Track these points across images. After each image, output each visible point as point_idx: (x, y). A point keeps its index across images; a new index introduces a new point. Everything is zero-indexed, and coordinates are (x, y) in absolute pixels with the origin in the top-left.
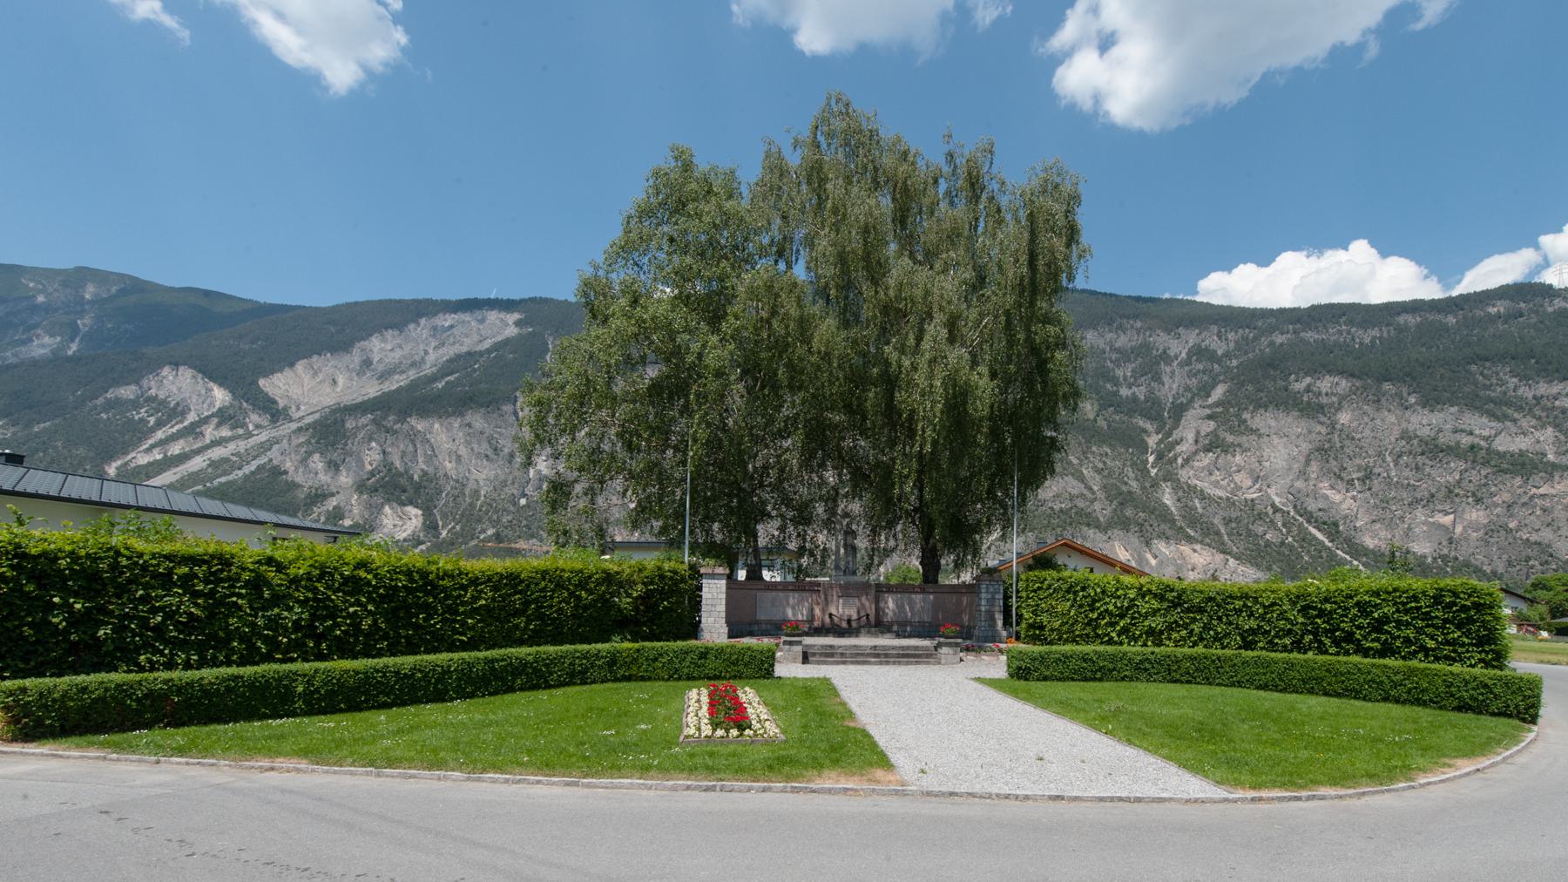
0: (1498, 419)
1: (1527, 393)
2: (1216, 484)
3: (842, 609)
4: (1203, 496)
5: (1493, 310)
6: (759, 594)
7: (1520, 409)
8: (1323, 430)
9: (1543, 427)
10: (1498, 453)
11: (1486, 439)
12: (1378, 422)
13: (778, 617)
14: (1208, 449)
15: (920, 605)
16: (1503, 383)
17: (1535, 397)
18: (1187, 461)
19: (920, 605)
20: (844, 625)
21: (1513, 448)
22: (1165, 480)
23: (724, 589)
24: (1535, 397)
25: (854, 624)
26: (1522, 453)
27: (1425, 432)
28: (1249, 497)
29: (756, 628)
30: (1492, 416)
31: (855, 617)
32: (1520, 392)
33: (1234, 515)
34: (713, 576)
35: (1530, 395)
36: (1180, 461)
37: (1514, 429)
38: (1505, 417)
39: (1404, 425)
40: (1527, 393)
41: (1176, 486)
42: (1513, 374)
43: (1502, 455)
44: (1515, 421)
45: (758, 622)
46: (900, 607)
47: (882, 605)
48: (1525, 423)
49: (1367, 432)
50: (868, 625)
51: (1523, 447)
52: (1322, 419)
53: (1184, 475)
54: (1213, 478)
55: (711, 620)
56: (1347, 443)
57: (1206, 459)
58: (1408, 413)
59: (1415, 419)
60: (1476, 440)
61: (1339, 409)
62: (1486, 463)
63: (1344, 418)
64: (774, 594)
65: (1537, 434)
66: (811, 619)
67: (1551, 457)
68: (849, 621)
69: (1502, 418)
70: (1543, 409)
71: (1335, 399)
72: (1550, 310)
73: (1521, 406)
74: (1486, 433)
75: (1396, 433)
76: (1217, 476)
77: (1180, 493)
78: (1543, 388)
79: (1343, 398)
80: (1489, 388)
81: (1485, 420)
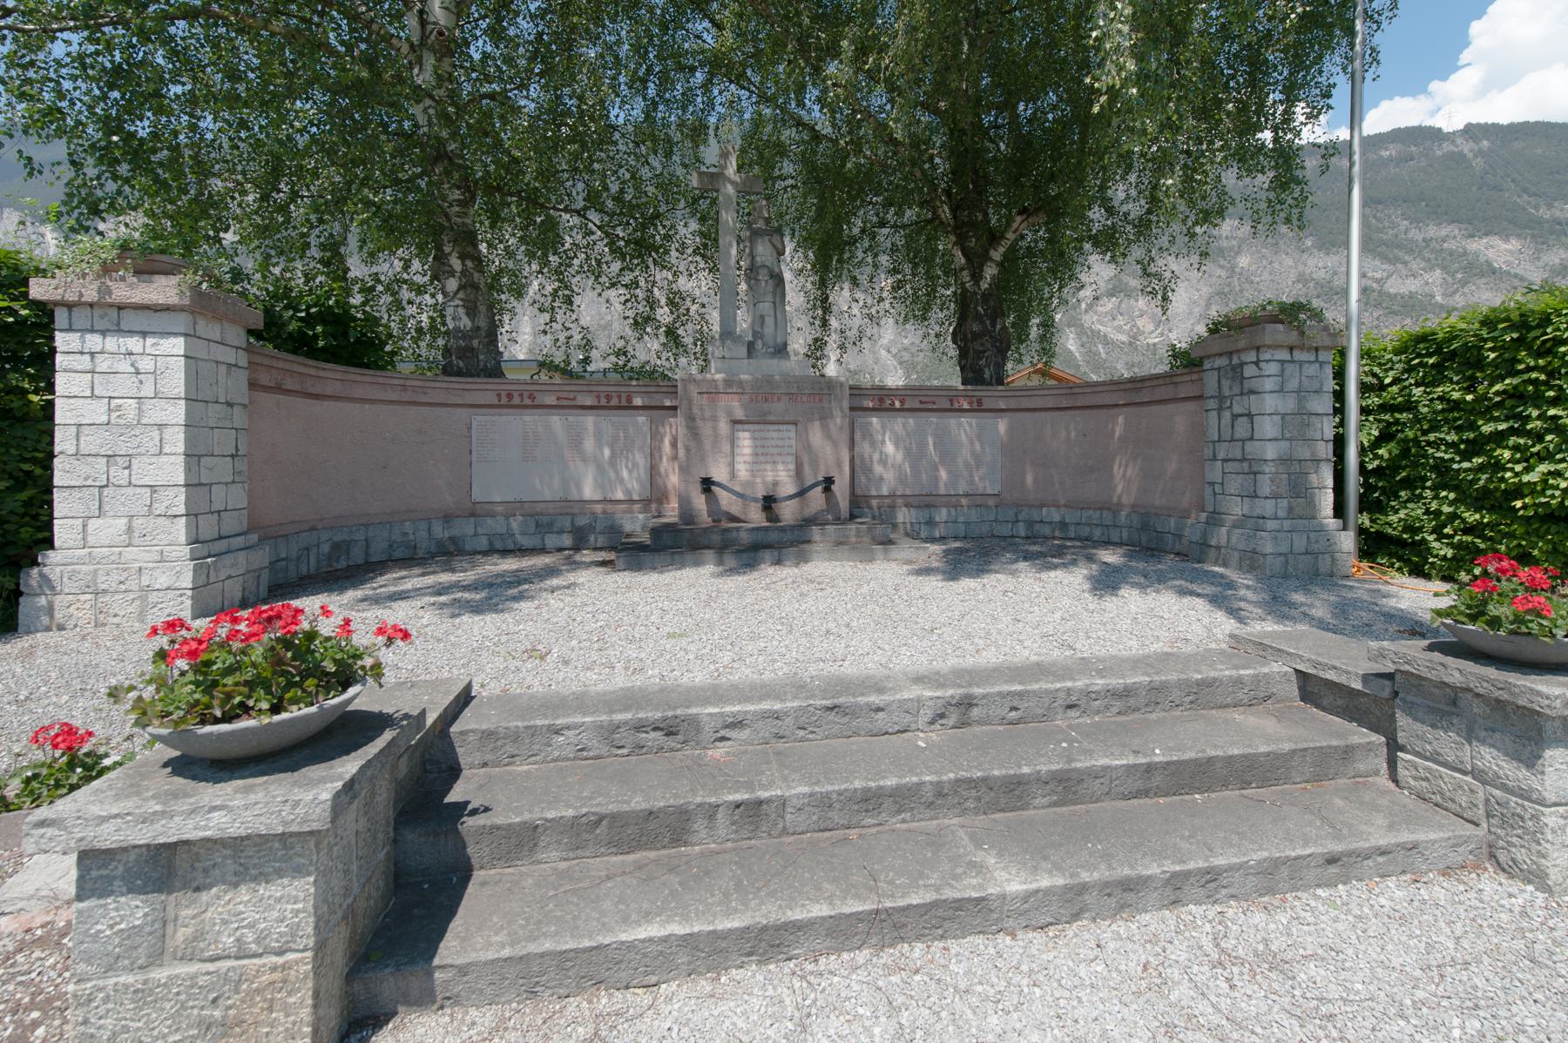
0: (1390, 261)
1: (1416, 235)
2: (1119, 329)
3: (747, 465)
4: (1106, 341)
5: (1385, 154)
6: (479, 420)
7: (1410, 251)
8: (1223, 274)
9: (1432, 269)
10: (1389, 295)
11: (1378, 281)
12: (1276, 265)
13: (546, 489)
14: (1111, 294)
15: (971, 451)
16: (1394, 226)
17: (1424, 240)
18: (1090, 306)
19: (971, 451)
20: (756, 516)
21: (1404, 290)
22: (1069, 326)
23: (176, 380)
24: (1424, 240)
25: (788, 512)
26: (1412, 295)
27: (1322, 274)
28: (1151, 341)
29: (464, 528)
30: (1385, 258)
31: (788, 488)
32: (1410, 235)
33: (1136, 360)
34: (115, 317)
35: (1420, 238)
36: (1083, 306)
37: (1404, 272)
38: (1396, 260)
39: (1301, 268)
40: (1416, 235)
41: (1081, 331)
42: (1405, 217)
43: (1393, 297)
44: (1405, 263)
45: (475, 512)
46: (915, 456)
47: (864, 448)
48: (1415, 266)
49: (1266, 276)
50: (831, 517)
51: (1413, 288)
52: (1222, 262)
53: (1088, 320)
54: (1116, 323)
55: (107, 530)
56: (1247, 286)
57: (1108, 305)
58: (1305, 256)
59: (1311, 262)
60: (1369, 283)
61: (1238, 253)
62: (1377, 305)
63: (1243, 261)
64: (530, 419)
65: (1426, 276)
66: (655, 496)
67: (1438, 298)
68: (769, 502)
69: (1393, 261)
70: (1432, 251)
71: (1234, 243)
72: (1439, 153)
73: (1412, 248)
74: (1378, 275)
75: (1293, 277)
76: (1120, 320)
77: (1084, 339)
78: (1432, 231)
79: (1242, 241)
80: (1381, 230)
81: (1377, 262)
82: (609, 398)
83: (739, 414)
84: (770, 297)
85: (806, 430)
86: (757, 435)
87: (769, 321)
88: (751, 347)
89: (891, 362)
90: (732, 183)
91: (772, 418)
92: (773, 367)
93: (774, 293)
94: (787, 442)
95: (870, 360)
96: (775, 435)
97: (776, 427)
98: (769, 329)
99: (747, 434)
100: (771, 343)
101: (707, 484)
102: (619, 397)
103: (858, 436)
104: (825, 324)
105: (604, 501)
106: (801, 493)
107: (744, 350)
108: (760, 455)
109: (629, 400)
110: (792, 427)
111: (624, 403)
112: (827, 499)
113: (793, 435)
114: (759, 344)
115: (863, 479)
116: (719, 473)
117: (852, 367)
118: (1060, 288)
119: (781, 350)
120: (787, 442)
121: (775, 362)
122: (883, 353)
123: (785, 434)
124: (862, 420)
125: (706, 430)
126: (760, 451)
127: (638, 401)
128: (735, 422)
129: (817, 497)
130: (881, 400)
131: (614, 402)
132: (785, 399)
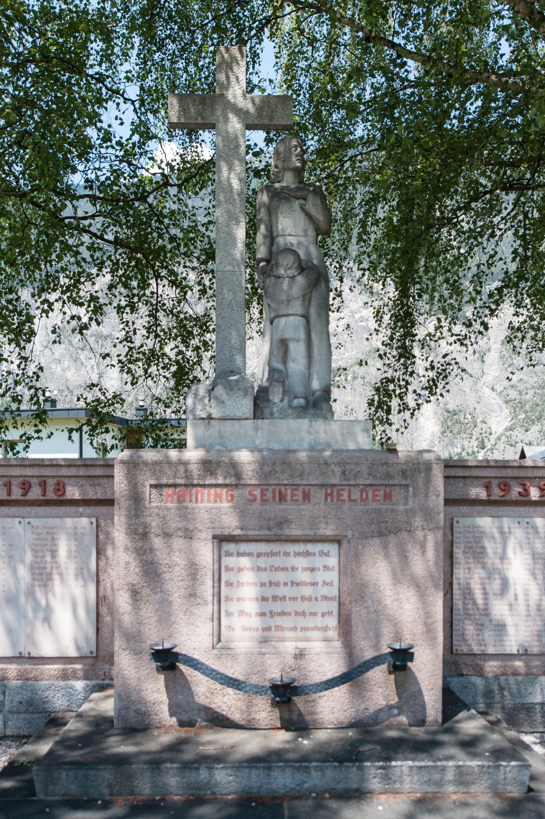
31: (326, 662)
47: (471, 576)
82: (26, 487)
83: (230, 523)
84: (297, 307)
85: (357, 556)
86: (262, 562)
87: (297, 350)
88: (261, 402)
89: (495, 400)
90: (239, 112)
91: (296, 532)
92: (299, 434)
93: (306, 298)
94: (320, 576)
95: (471, 399)
96: (301, 562)
97: (300, 547)
98: (297, 365)
99: (245, 562)
100: (299, 388)
101: (167, 660)
102: (43, 485)
103: (458, 553)
104: (406, 354)
105: (19, 658)
106: (353, 675)
107: (245, 406)
108: (271, 604)
109: (60, 488)
110: (333, 548)
111: (51, 495)
112: (400, 687)
113: (333, 561)
114: (276, 397)
115: (470, 629)
116: (192, 638)
117: (451, 407)
118: (185, 399)
119: (318, 403)
120: (320, 576)
121: (304, 423)
122: (487, 391)
123: (318, 562)
124: (468, 521)
125: (173, 559)
126: (270, 592)
127: (73, 492)
128: (221, 539)
129: (380, 687)
130: (505, 487)
131: (35, 493)
132: (318, 495)
